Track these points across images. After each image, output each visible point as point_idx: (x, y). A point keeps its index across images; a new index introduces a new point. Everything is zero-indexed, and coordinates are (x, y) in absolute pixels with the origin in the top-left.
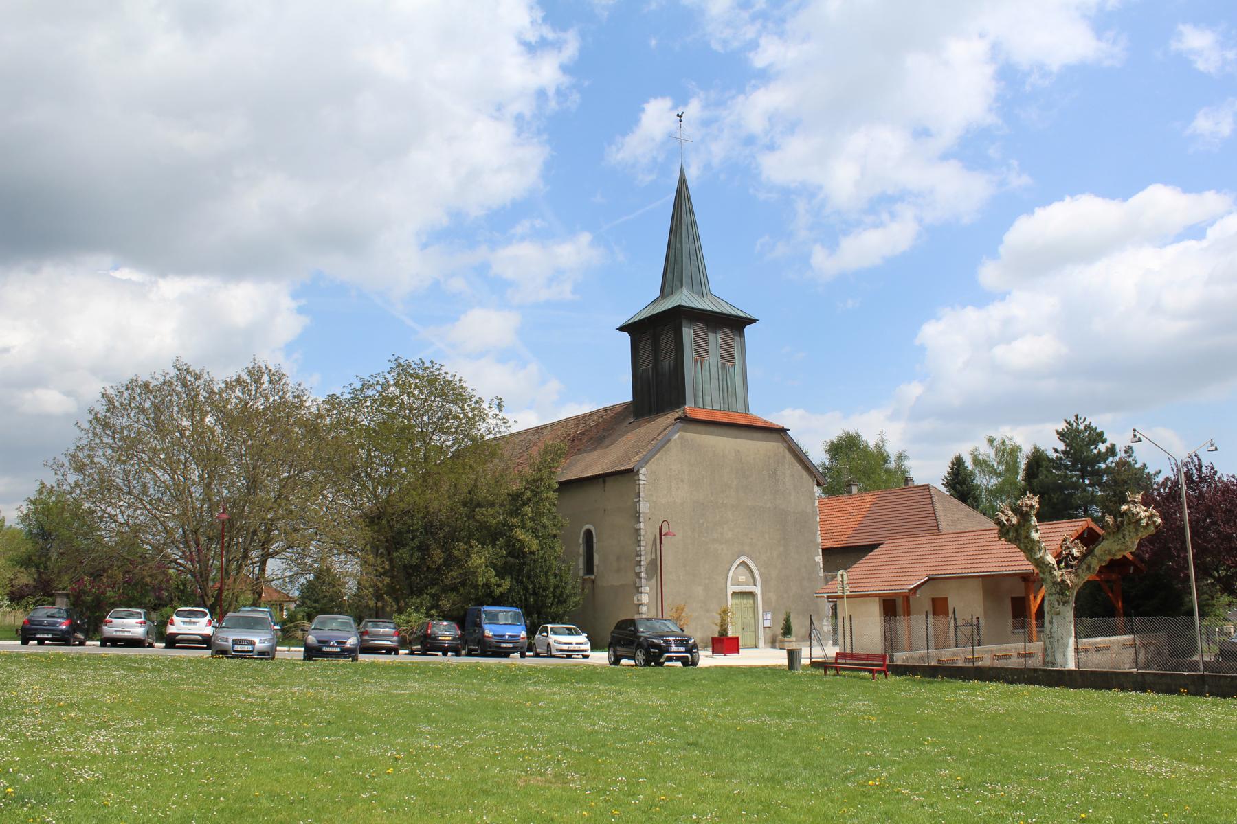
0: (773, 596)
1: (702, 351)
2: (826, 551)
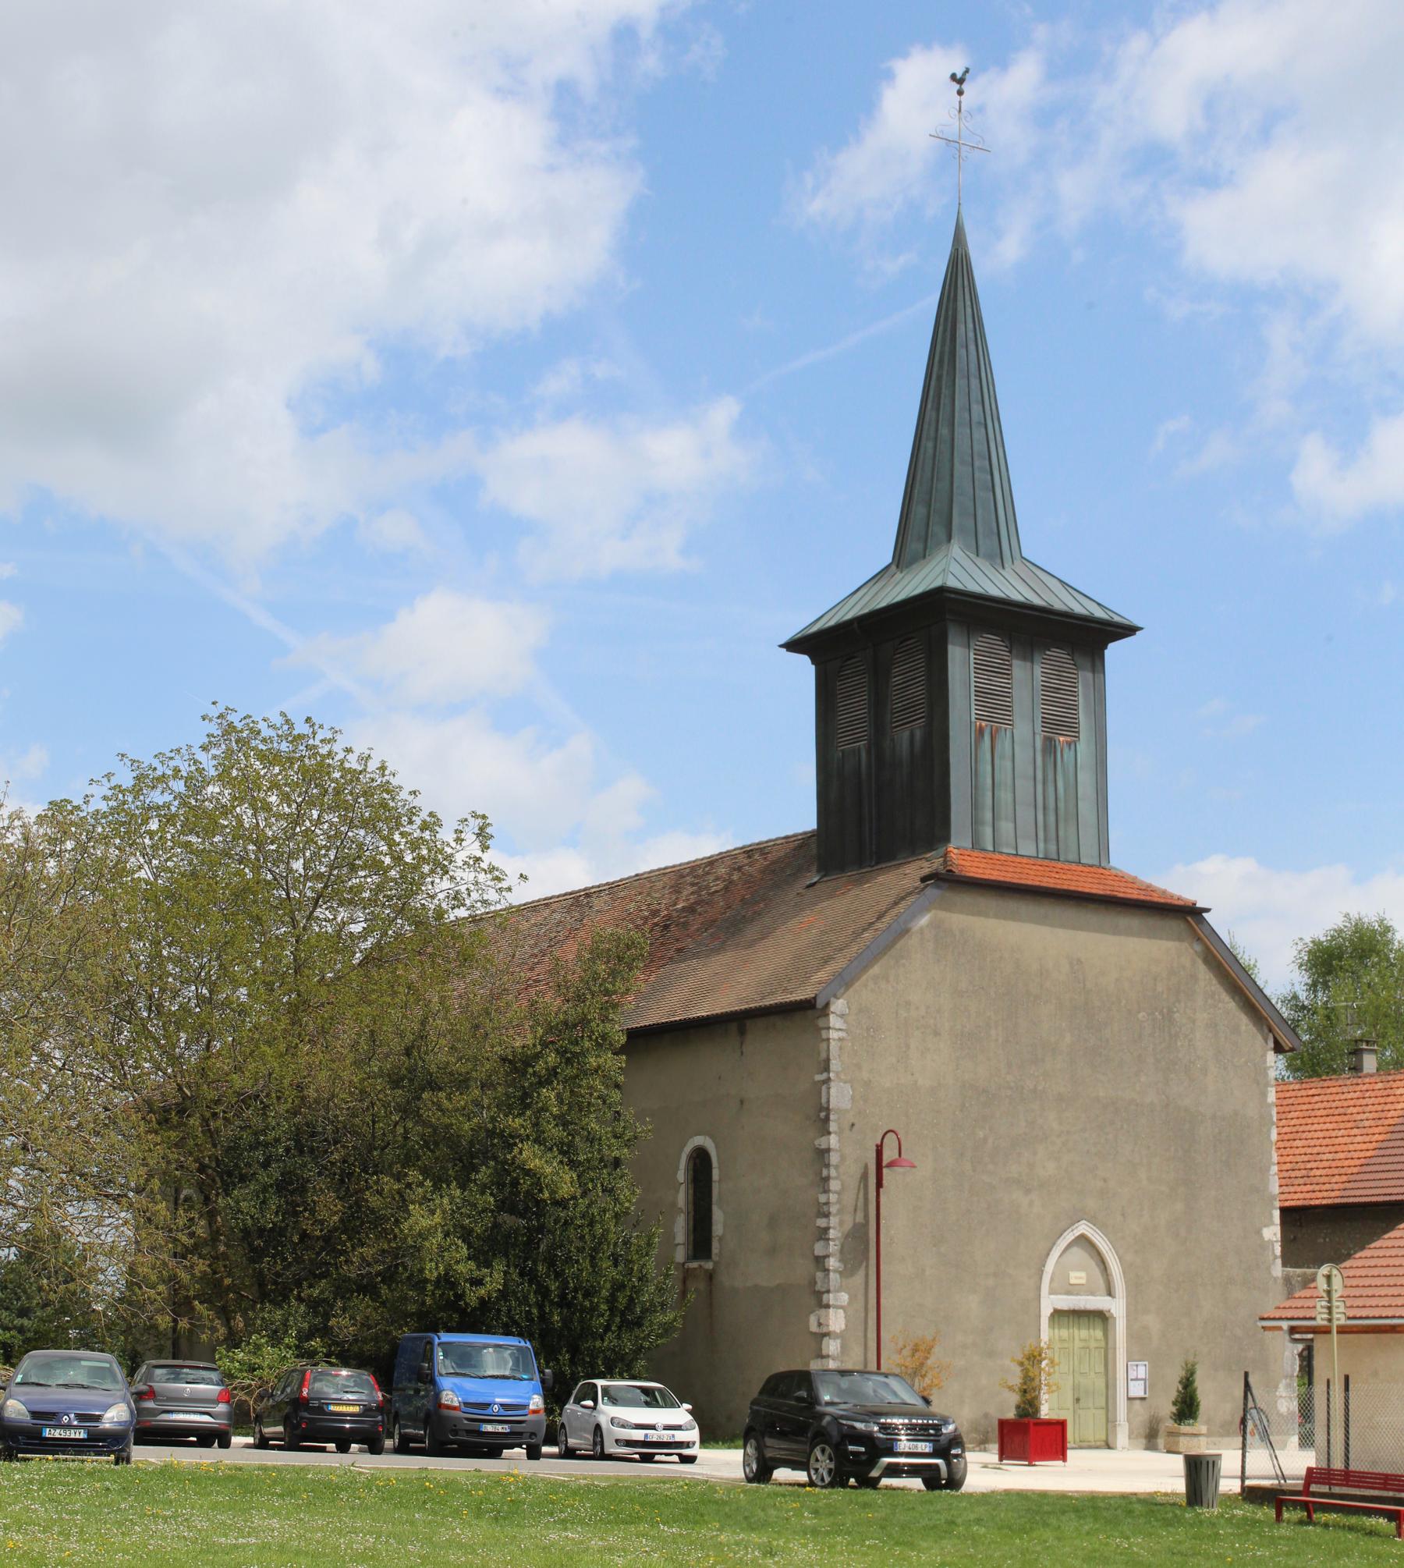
0: (1152, 1322)
1: (995, 704)
2: (1294, 1218)
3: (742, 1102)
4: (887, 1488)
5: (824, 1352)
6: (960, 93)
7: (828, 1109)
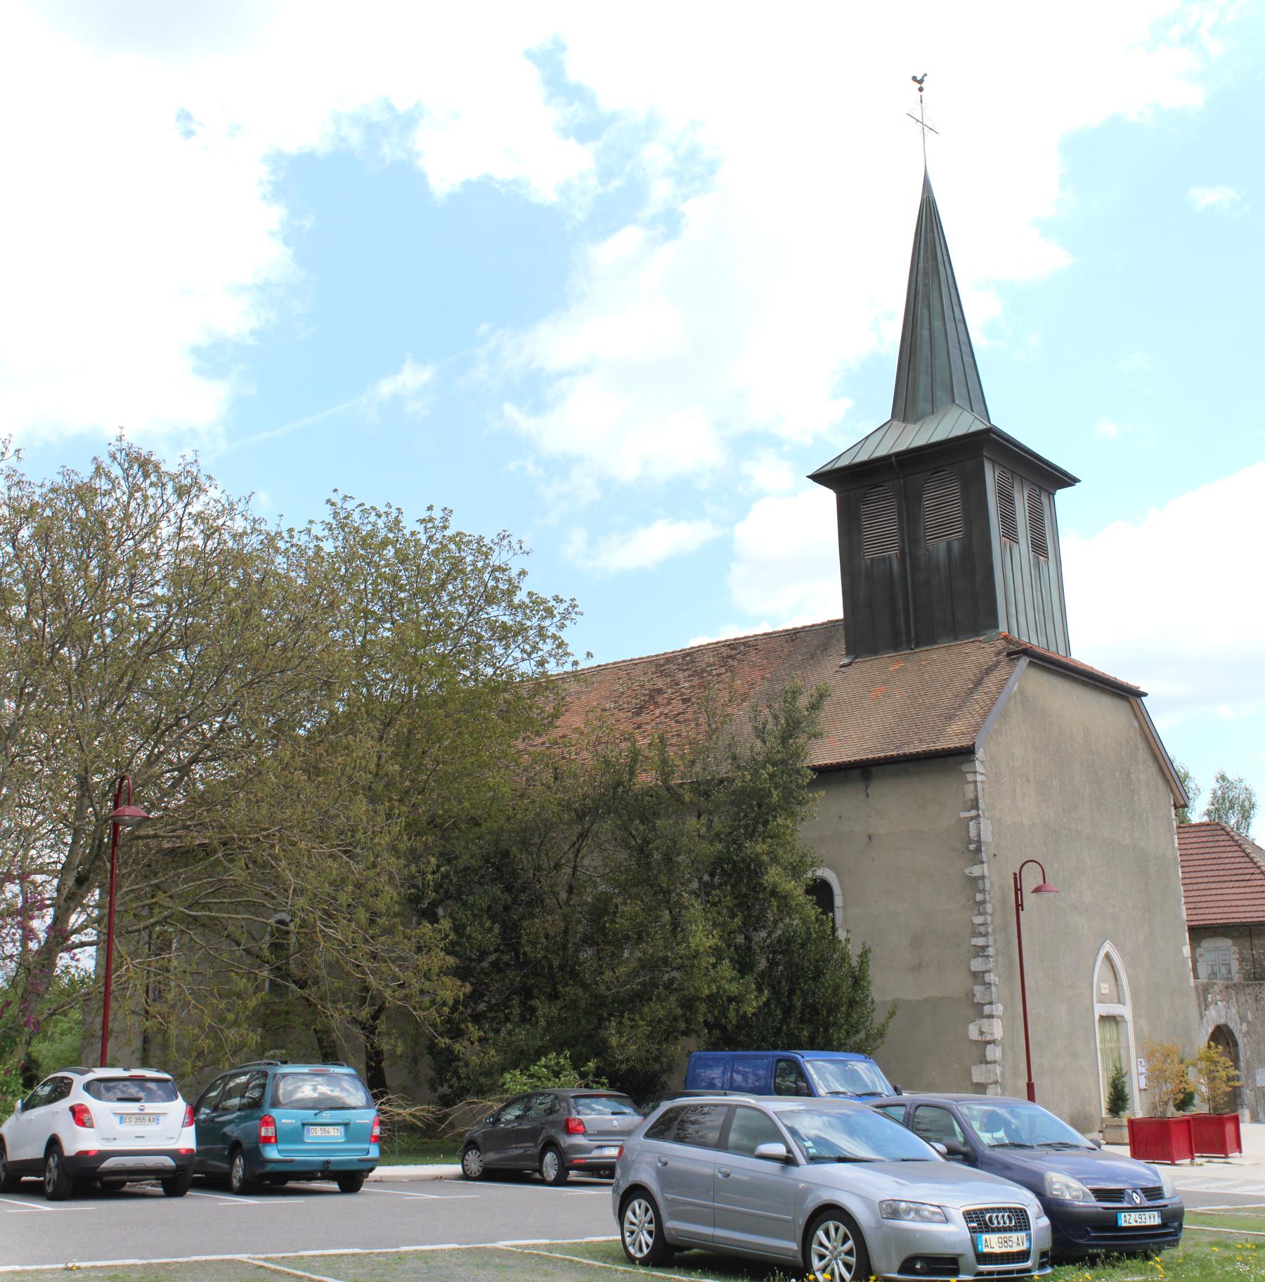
3: (870, 838)
4: (379, 1181)
5: (989, 1058)
6: (921, 90)
7: (979, 842)
